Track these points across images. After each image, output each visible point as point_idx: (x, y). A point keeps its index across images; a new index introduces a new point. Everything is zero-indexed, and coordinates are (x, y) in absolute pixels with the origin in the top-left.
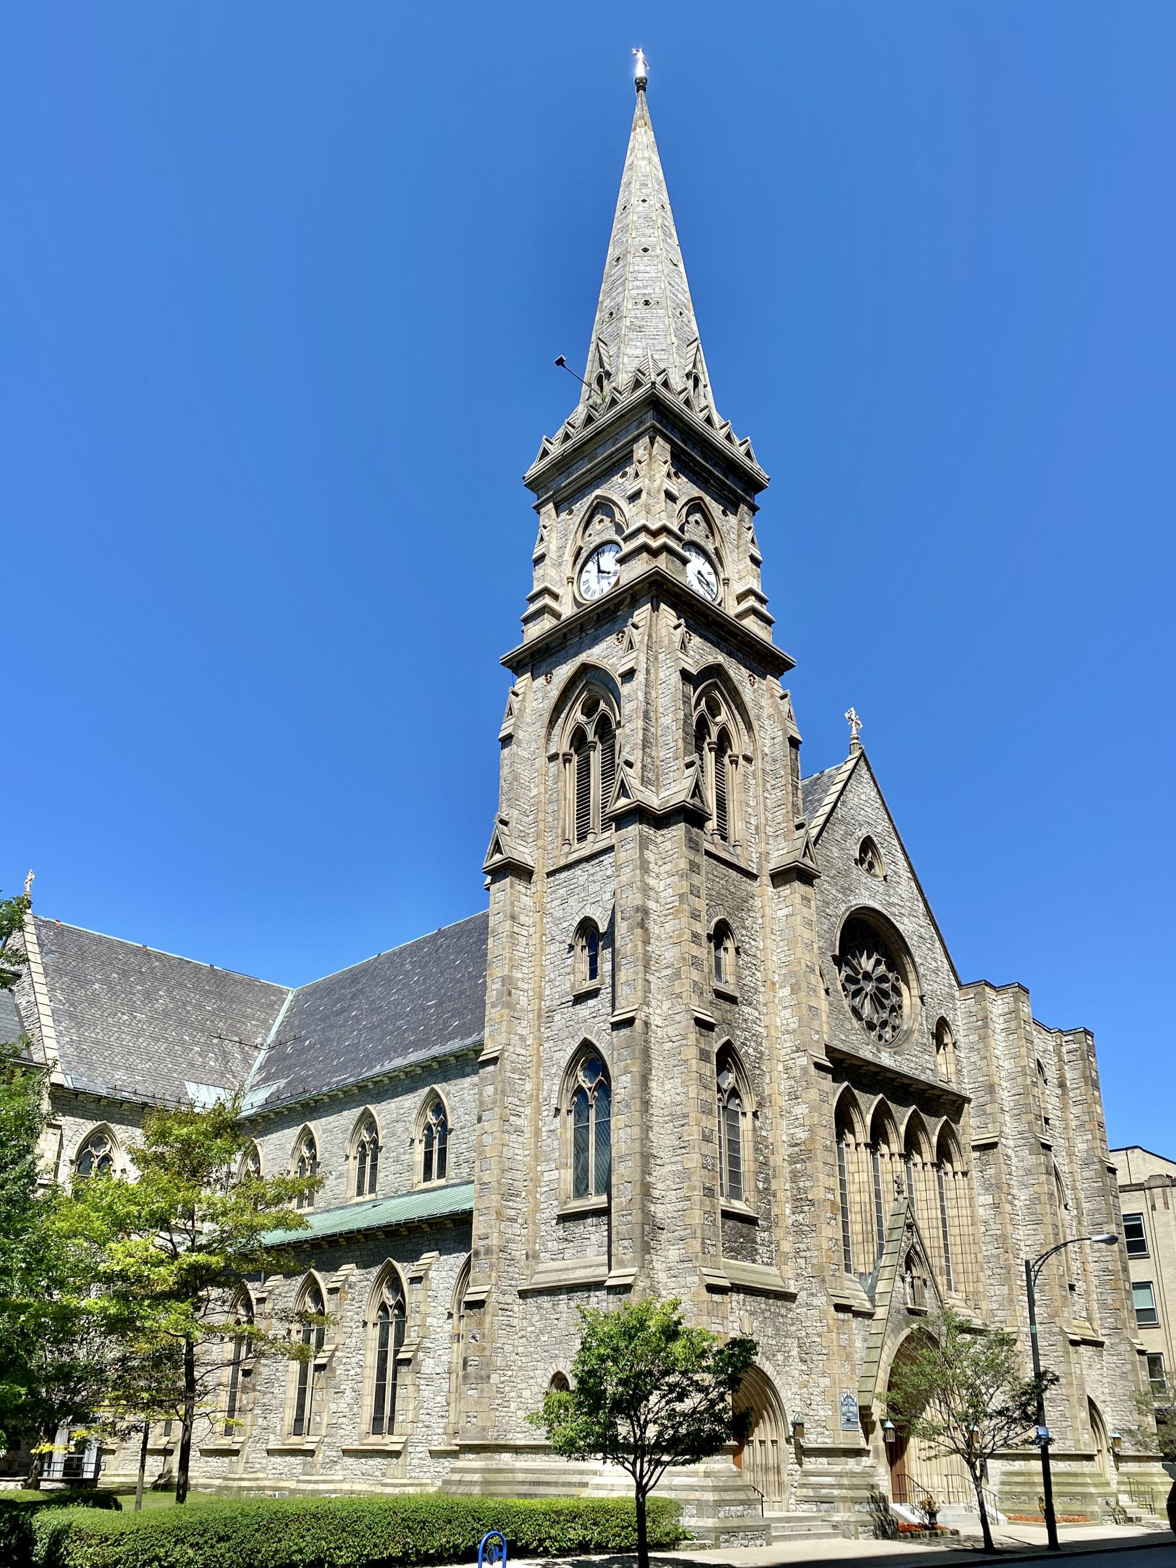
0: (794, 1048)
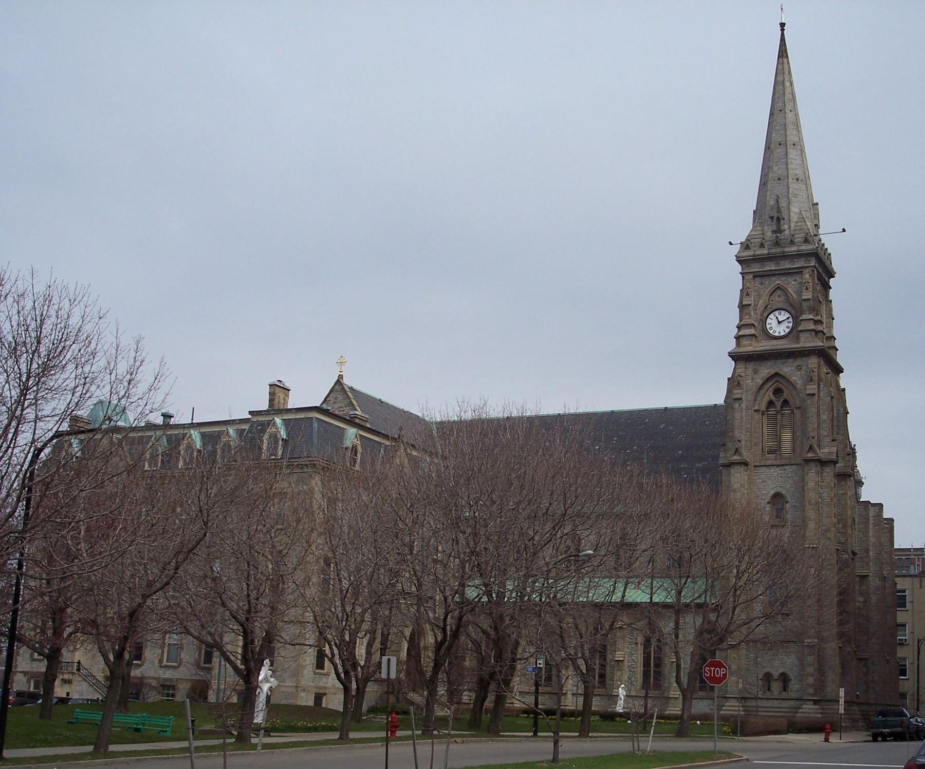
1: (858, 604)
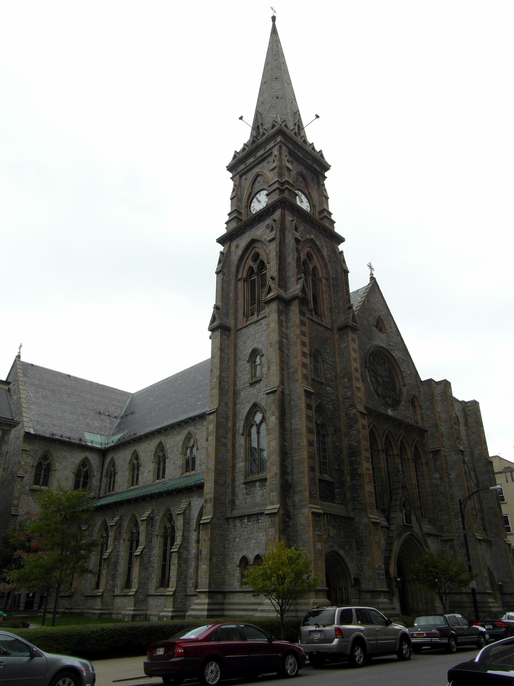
0: (350, 405)
1: (435, 481)
